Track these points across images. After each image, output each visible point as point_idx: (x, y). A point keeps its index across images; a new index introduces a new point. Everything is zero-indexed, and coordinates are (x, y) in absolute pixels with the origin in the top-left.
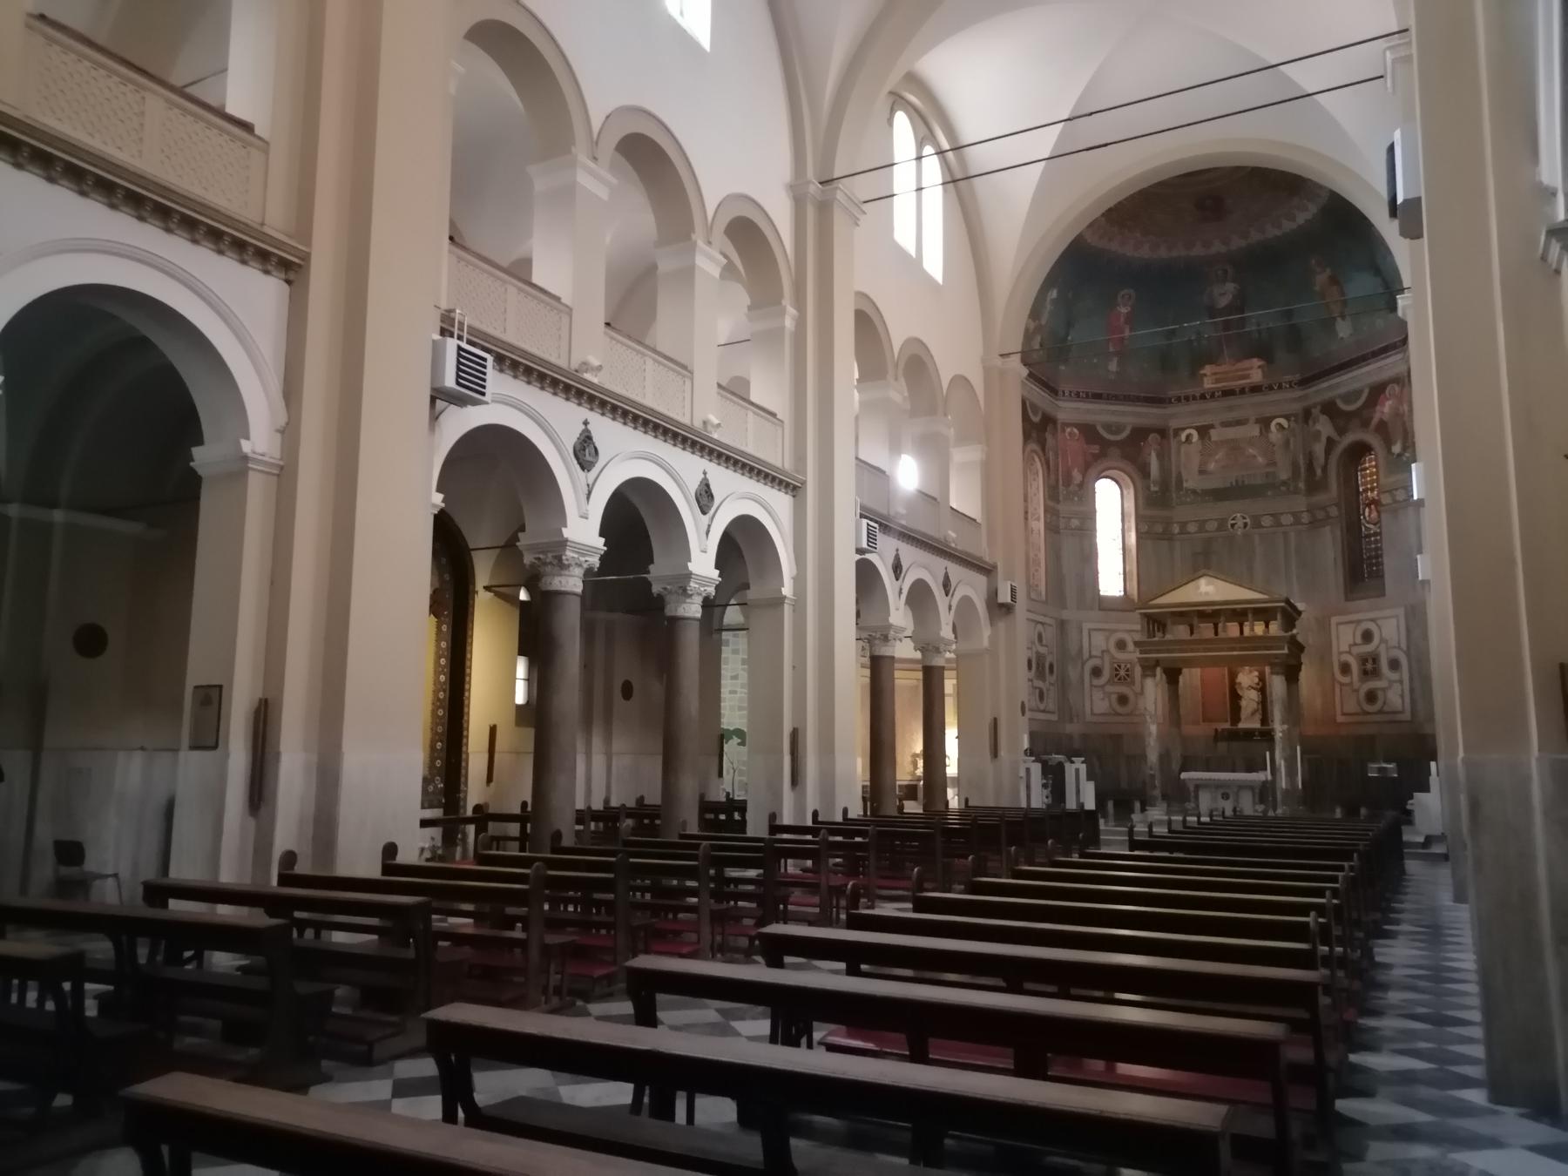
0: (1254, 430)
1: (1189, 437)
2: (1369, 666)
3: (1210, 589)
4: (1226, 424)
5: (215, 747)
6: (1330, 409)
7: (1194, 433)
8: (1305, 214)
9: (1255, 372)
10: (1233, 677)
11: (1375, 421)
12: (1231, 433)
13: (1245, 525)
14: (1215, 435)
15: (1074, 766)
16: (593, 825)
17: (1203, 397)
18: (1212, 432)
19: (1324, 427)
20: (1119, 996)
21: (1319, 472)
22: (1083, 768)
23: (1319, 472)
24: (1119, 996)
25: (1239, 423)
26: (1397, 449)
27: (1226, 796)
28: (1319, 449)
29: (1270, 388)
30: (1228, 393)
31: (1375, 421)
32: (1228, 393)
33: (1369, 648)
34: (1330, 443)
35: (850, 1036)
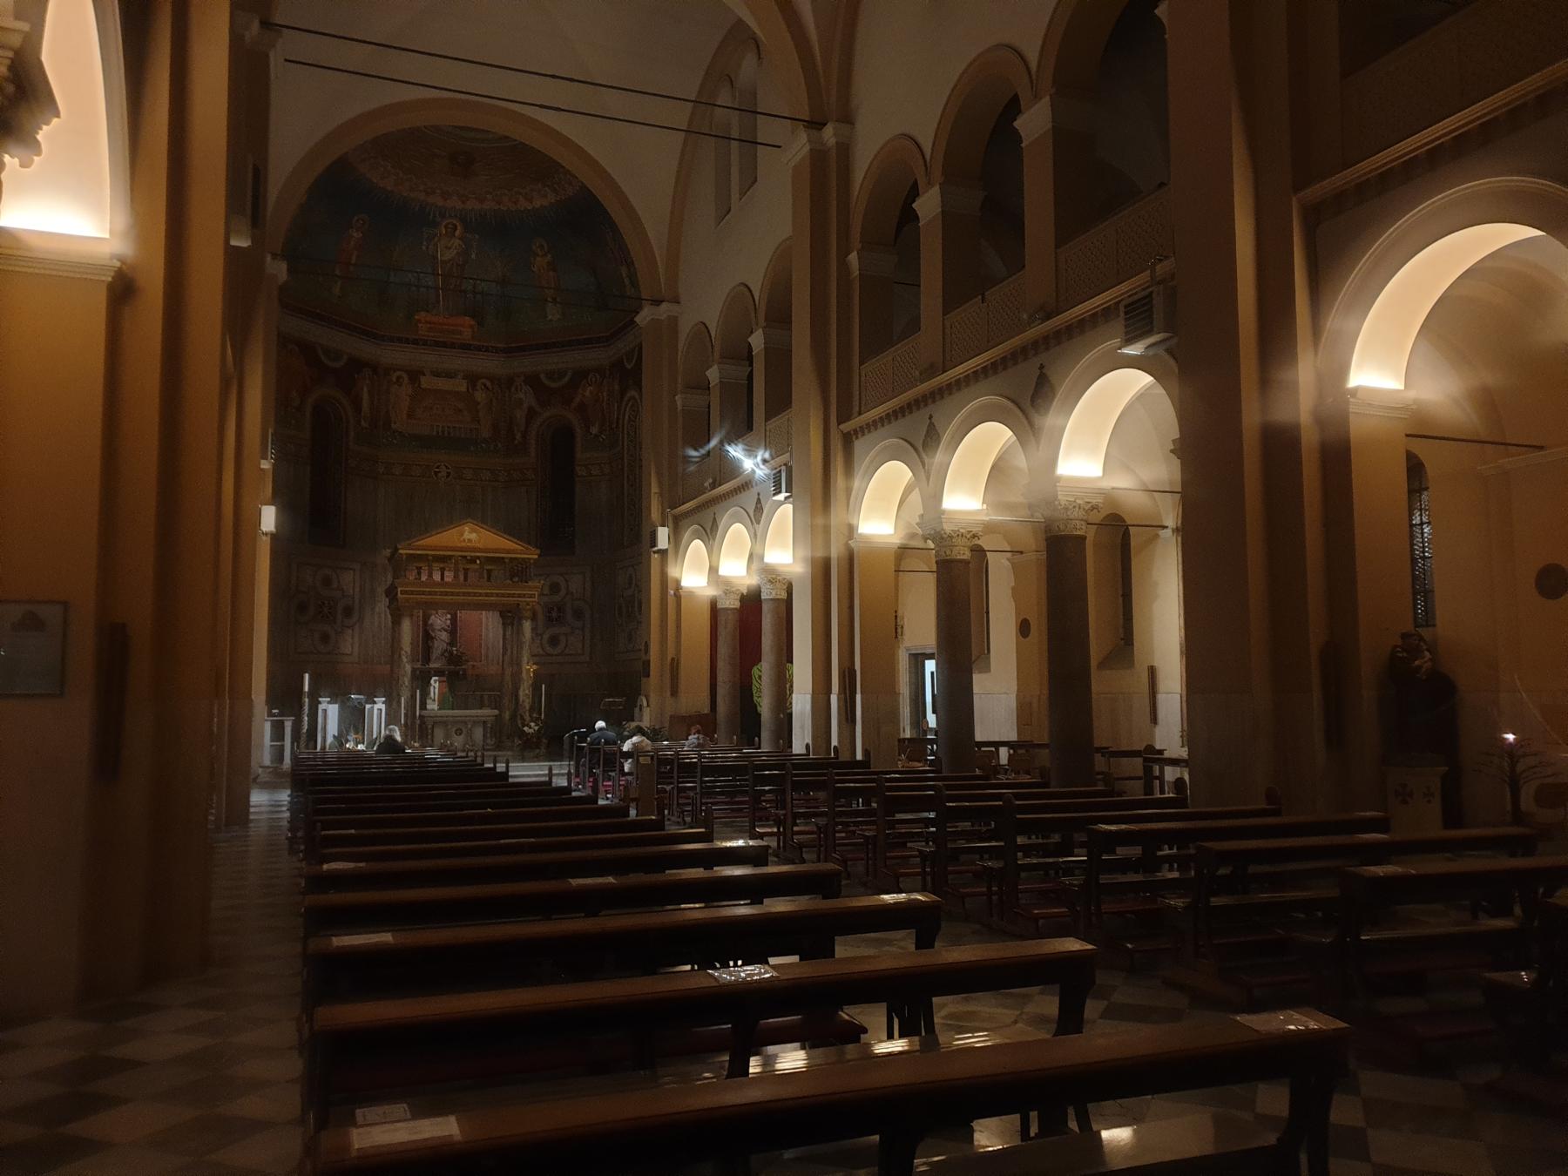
0: (462, 386)
1: (398, 378)
2: (554, 614)
3: (473, 536)
4: (437, 374)
5: (339, 186)
6: (533, 380)
7: (405, 376)
8: (542, 200)
9: (466, 328)
10: (426, 618)
11: (577, 400)
12: (442, 384)
13: (449, 474)
14: (426, 382)
15: (376, 707)
16: (1192, 851)
17: (416, 342)
18: (423, 379)
19: (525, 396)
20: (896, 1021)
21: (518, 437)
22: (383, 707)
23: (518, 437)
24: (896, 1021)
25: (450, 375)
26: (594, 430)
27: (459, 732)
28: (520, 415)
29: (479, 349)
30: (437, 344)
31: (577, 400)
32: (437, 344)
33: (557, 598)
34: (531, 414)
35: (419, 1113)
